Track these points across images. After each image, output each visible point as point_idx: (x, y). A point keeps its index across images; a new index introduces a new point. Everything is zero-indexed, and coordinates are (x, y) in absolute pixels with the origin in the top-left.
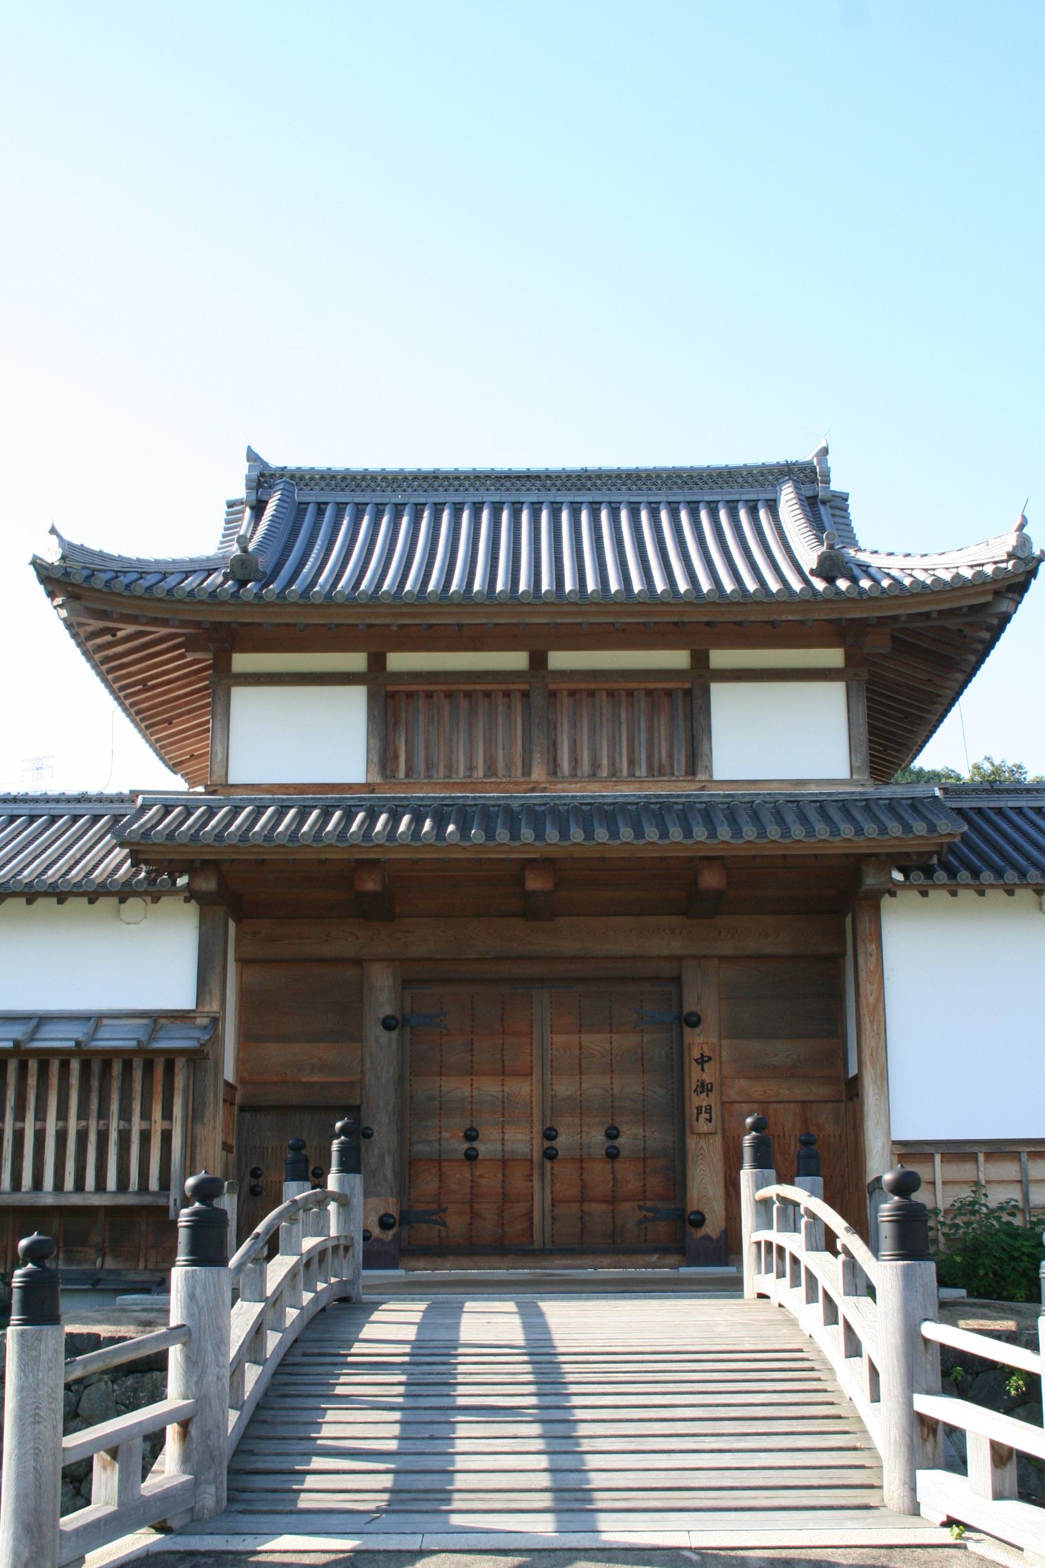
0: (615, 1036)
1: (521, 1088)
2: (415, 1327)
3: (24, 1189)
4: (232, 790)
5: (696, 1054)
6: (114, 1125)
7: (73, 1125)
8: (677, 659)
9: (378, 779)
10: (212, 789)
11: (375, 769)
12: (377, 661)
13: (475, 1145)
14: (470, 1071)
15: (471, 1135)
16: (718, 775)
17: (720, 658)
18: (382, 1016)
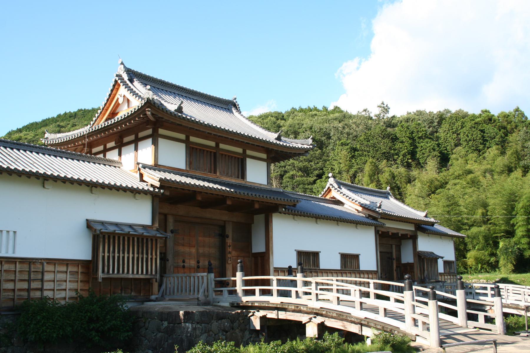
0: (210, 239)
1: (193, 250)
2: (279, 312)
3: (125, 273)
4: (160, 166)
5: (228, 245)
6: (145, 256)
7: (136, 256)
8: (240, 150)
9: (188, 169)
10: (156, 165)
11: (188, 166)
12: (188, 138)
13: (185, 264)
14: (183, 245)
15: (184, 262)
16: (248, 180)
17: (249, 152)
18: (171, 229)
